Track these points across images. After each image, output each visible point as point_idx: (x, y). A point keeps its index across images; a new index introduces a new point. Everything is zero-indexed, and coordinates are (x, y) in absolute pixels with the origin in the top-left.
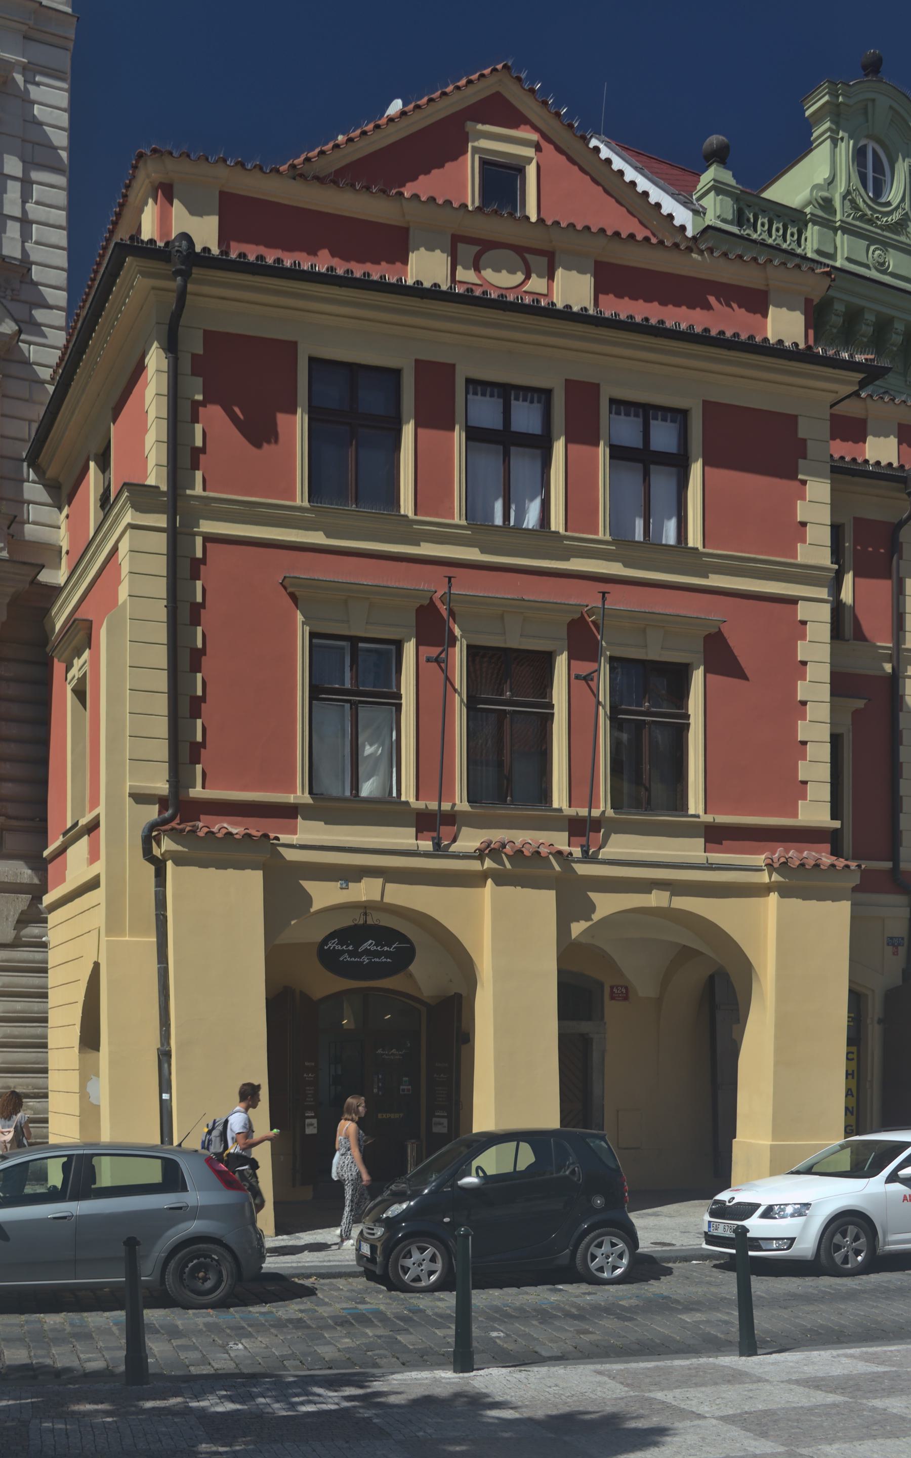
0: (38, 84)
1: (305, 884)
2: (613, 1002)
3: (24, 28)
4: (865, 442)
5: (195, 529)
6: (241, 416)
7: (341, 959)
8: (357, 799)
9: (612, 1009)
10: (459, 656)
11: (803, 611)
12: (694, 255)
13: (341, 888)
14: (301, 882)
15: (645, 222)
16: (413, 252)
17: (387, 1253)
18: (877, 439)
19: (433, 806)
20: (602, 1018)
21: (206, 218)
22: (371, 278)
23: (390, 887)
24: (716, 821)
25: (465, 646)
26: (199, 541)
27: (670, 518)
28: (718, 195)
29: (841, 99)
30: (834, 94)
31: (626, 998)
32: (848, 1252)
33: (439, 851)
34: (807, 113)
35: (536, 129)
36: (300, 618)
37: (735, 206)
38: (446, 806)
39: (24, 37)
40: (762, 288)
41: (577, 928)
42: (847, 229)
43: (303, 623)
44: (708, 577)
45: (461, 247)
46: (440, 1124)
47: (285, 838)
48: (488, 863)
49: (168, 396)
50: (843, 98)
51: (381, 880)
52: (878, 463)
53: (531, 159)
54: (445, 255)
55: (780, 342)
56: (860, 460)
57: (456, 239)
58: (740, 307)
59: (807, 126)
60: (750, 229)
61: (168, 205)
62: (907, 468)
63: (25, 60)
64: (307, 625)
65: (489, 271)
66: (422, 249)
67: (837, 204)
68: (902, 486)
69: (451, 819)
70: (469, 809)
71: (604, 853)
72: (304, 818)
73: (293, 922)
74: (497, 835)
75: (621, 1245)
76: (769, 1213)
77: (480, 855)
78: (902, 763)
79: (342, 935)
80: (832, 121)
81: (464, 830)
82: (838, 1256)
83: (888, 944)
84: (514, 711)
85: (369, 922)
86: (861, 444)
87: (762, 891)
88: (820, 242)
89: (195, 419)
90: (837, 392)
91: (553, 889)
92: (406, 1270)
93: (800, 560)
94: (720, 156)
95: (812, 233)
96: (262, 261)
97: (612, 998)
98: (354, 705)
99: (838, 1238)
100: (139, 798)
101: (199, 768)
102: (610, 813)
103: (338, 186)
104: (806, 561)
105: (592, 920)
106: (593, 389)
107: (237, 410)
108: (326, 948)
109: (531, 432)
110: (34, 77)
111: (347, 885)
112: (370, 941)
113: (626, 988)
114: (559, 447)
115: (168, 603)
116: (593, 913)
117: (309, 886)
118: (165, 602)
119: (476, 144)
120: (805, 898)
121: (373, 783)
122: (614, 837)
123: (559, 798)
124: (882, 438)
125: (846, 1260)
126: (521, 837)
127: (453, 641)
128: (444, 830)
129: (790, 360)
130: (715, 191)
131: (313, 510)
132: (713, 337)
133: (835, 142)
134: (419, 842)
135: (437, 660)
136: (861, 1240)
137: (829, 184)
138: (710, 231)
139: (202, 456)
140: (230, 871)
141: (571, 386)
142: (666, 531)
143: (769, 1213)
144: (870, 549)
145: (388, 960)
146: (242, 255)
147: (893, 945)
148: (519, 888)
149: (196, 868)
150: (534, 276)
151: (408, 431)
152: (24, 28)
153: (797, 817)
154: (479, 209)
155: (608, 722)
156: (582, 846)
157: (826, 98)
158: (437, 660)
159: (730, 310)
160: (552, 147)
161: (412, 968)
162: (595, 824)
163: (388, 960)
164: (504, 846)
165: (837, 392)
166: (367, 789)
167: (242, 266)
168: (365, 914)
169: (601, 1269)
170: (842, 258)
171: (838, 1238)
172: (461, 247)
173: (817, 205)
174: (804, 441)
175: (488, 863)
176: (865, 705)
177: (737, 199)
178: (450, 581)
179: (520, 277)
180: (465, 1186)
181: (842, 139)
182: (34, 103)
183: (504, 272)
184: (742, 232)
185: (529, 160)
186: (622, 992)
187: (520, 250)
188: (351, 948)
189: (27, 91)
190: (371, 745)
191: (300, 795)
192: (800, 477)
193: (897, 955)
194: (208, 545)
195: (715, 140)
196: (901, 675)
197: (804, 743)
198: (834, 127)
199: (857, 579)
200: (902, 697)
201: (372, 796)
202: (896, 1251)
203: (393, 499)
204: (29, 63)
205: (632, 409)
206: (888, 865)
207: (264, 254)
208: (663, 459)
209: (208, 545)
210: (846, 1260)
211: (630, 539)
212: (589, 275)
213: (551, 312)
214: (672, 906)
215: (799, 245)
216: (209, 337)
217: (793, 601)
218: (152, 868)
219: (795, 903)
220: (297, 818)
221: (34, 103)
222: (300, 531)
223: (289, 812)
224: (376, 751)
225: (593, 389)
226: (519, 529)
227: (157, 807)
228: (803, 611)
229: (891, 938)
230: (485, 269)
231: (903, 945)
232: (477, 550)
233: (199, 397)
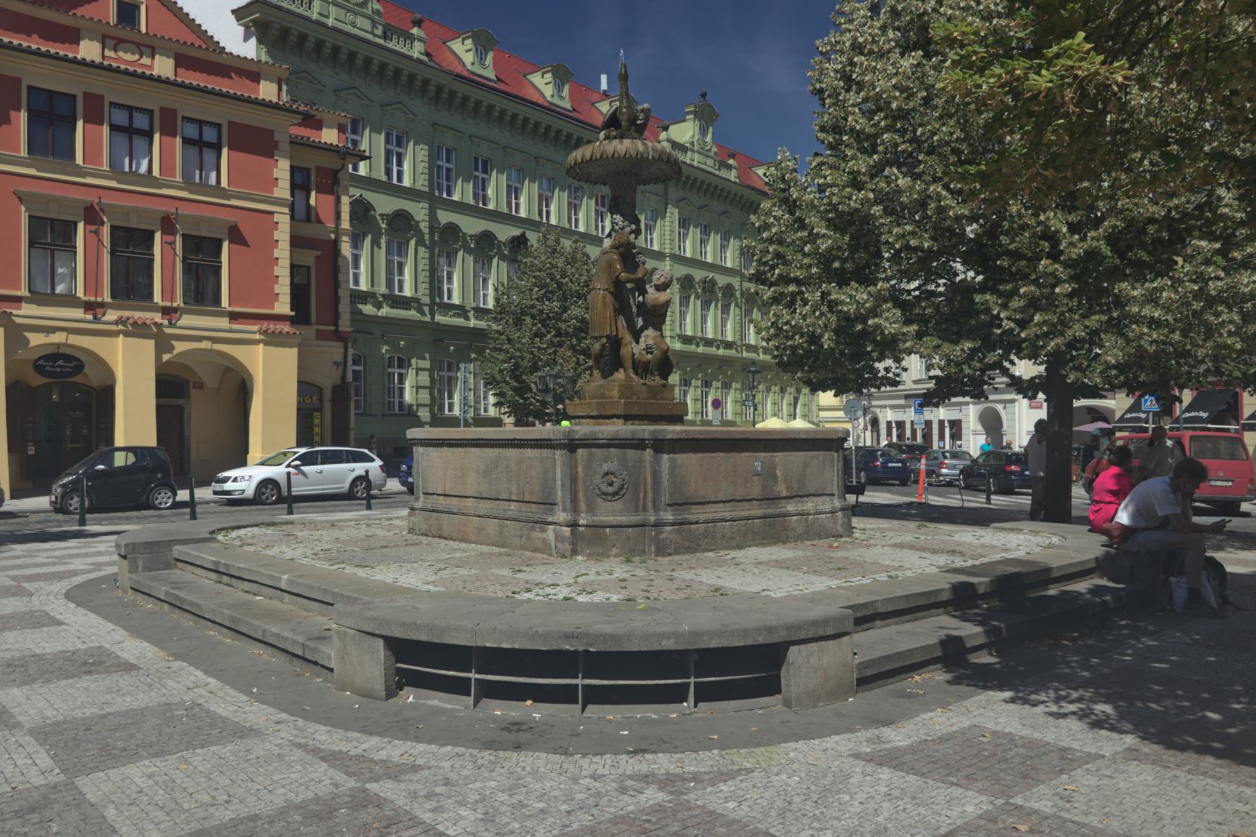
1: (26, 334)
9: (194, 393)
11: (277, 218)
17: (63, 497)
19: (93, 299)
20: (189, 397)
23: (70, 336)
31: (201, 388)
33: (96, 320)
36: (23, 209)
38: (99, 299)
41: (166, 357)
47: (14, 312)
48: (120, 327)
69: (102, 305)
74: (125, 314)
75: (169, 494)
76: (235, 480)
77: (116, 323)
79: (46, 358)
81: (109, 311)
82: (264, 497)
87: (257, 342)
92: (71, 505)
93: (275, 195)
97: (194, 387)
98: (52, 251)
99: (263, 490)
102: (182, 305)
114: (157, 137)
117: (28, 335)
122: (184, 316)
123: (157, 298)
125: (267, 499)
126: (138, 315)
127: (102, 223)
128: (98, 310)
135: (95, 232)
143: (235, 480)
151: (80, 124)
154: (116, 25)
158: (95, 232)
161: (86, 370)
162: (175, 310)
164: (128, 319)
166: (59, 289)
171: (263, 490)
172: (107, 40)
174: (277, 142)
175: (120, 327)
179: (137, 57)
187: (138, 45)
191: (24, 292)
200: (340, 251)
206: (333, 328)
208: (210, 145)
210: (267, 499)
217: (272, 213)
223: (18, 300)
226: (136, 174)
228: (277, 218)
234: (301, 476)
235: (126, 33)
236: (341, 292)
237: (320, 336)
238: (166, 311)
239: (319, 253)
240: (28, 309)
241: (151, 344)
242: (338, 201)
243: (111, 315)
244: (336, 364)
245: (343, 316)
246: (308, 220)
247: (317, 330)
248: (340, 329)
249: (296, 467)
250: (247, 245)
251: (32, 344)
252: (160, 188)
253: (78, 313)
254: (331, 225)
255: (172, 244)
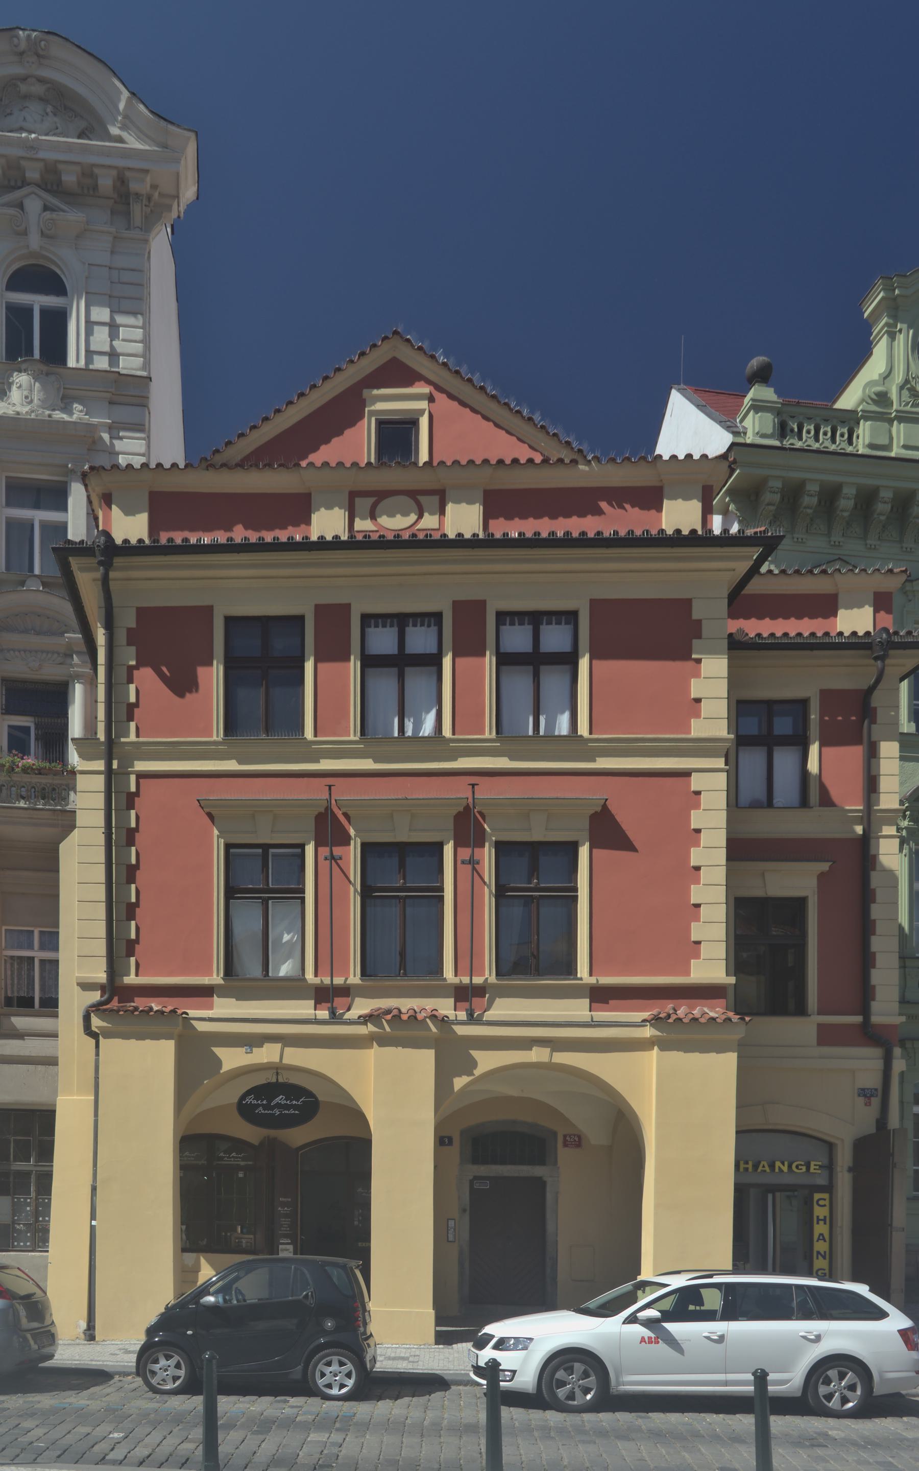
0: (121, 438)
2: (566, 1148)
3: (108, 395)
4: (835, 615)
5: (129, 769)
6: (168, 674)
7: (257, 1112)
8: (267, 978)
9: (564, 1155)
10: (353, 854)
12: (581, 467)
13: (246, 1053)
14: (213, 1048)
15: (535, 446)
16: (314, 513)
18: (849, 611)
20: (556, 1163)
21: (138, 516)
22: (266, 541)
23: (288, 1050)
24: (600, 982)
25: (359, 844)
26: (133, 778)
27: (563, 712)
28: (757, 413)
29: (897, 292)
30: (889, 289)
32: (574, 1388)
33: (335, 1018)
34: (866, 315)
35: (429, 382)
36: (216, 832)
37: (776, 420)
38: (339, 981)
39: (109, 403)
40: (658, 484)
41: (459, 1082)
42: (903, 418)
43: (218, 837)
44: (595, 761)
45: (358, 500)
46: (287, 1250)
47: (192, 1013)
49: (105, 665)
50: (899, 290)
51: (280, 1045)
52: (854, 634)
53: (424, 410)
54: (343, 511)
55: (678, 531)
56: (833, 634)
57: (353, 495)
58: (633, 506)
59: (866, 328)
60: (794, 438)
61: (109, 510)
62: (915, 634)
63: (110, 421)
64: (222, 838)
65: (385, 517)
66: (323, 509)
67: (894, 395)
68: (868, 652)
69: (345, 991)
70: (360, 982)
71: (489, 1015)
72: (218, 997)
73: (205, 1082)
78: (875, 921)
79: (256, 1091)
80: (889, 316)
82: (561, 1393)
83: (859, 1095)
84: (540, 895)
85: (280, 1080)
86: (832, 618)
88: (871, 436)
89: (130, 680)
90: (734, 570)
91: (432, 1049)
93: (694, 734)
94: (762, 376)
95: (864, 430)
96: (158, 543)
97: (565, 1145)
98: (265, 902)
100: (86, 986)
101: (133, 960)
102: (493, 979)
103: (244, 469)
104: (710, 734)
105: (474, 1075)
106: (480, 606)
107: (164, 669)
108: (244, 1102)
109: (428, 652)
110: (119, 433)
111: (252, 1050)
112: (281, 1097)
113: (579, 1137)
114: (584, 663)
115: (105, 830)
116: (475, 1069)
117: (219, 1051)
118: (103, 830)
119: (373, 408)
120: (686, 1051)
121: (289, 965)
122: (498, 1001)
124: (855, 610)
125: (571, 1396)
128: (338, 1001)
129: (672, 546)
130: (754, 409)
131: (224, 743)
132: (591, 539)
133: (892, 336)
134: (592, 1013)
136: (591, 1378)
137: (885, 378)
138: (735, 448)
139: (136, 710)
140: (148, 1041)
141: (458, 606)
142: (559, 723)
144: (840, 718)
145: (296, 1112)
146: (170, 540)
147: (865, 1096)
148: (400, 1048)
149: (120, 1040)
150: (426, 515)
151: (309, 666)
152: (108, 395)
153: (690, 976)
155: (493, 899)
156: (467, 1010)
157: (882, 294)
159: (623, 511)
160: (444, 396)
162: (480, 991)
163: (296, 1112)
165: (734, 570)
167: (171, 549)
168: (277, 1073)
169: (329, 1386)
170: (898, 446)
173: (870, 401)
174: (699, 622)
175: (371, 1028)
176: (830, 867)
177: (778, 413)
178: (330, 789)
179: (413, 517)
180: (204, 1304)
181: (900, 331)
182: (118, 454)
183: (398, 516)
184: (784, 443)
185: (422, 412)
186: (575, 1141)
187: (413, 494)
188: (265, 1102)
189: (112, 445)
190: (288, 934)
191: (216, 978)
192: (694, 656)
193: (870, 1105)
194: (141, 781)
195: (755, 362)
196: (872, 835)
197: (698, 906)
198: (891, 321)
199: (824, 749)
201: (288, 975)
202: (634, 1392)
203: (301, 728)
204: (113, 422)
205: (563, 618)
206: (858, 1019)
207: (188, 537)
209: (141, 781)
210: (571, 1396)
211: (524, 735)
212: (477, 505)
213: (444, 543)
214: (552, 1061)
215: (850, 442)
216: (141, 612)
217: (686, 774)
218: (94, 1041)
219: (676, 1057)
220: (213, 996)
221: (118, 454)
222: (216, 761)
223: (206, 992)
224: (293, 937)
225: (480, 606)
226: (551, 738)
227: (99, 992)
228: (696, 782)
229: (863, 1090)
230: (380, 516)
231: (877, 1096)
232: (370, 761)
233: (133, 663)
234: (662, 1345)
235: (393, 477)
236: (877, 944)
237: (827, 1036)
238: (463, 994)
239: (825, 866)
240: (224, 1007)
241: (426, 1058)
242: (872, 753)
243: (361, 1007)
244: (865, 1094)
245: (880, 994)
246: (804, 803)
247: (820, 1027)
248: (875, 1019)
249: (649, 1323)
250: (634, 849)
251: (226, 1067)
252: (454, 759)
253: (305, 1008)
254: (856, 807)
255: (473, 863)
